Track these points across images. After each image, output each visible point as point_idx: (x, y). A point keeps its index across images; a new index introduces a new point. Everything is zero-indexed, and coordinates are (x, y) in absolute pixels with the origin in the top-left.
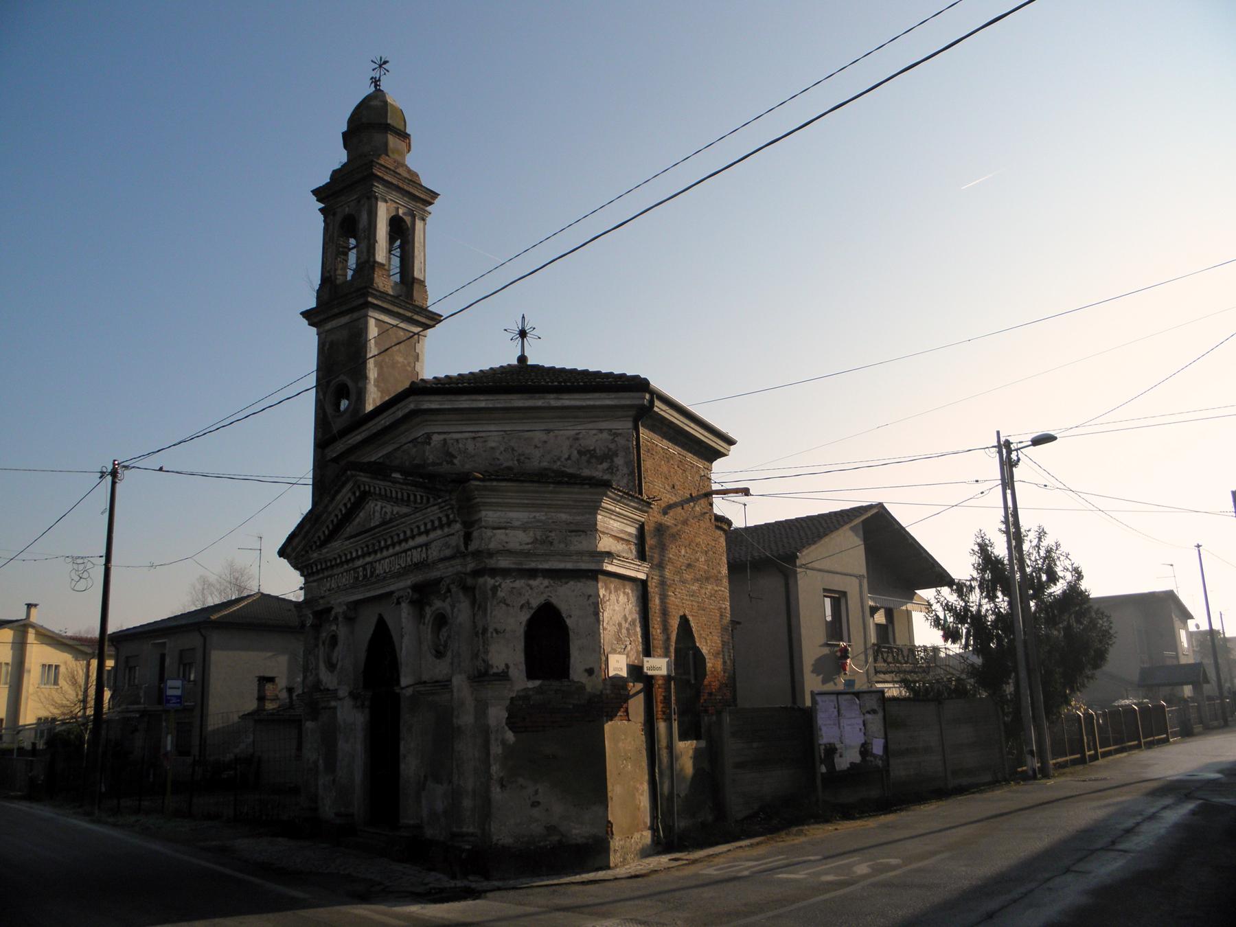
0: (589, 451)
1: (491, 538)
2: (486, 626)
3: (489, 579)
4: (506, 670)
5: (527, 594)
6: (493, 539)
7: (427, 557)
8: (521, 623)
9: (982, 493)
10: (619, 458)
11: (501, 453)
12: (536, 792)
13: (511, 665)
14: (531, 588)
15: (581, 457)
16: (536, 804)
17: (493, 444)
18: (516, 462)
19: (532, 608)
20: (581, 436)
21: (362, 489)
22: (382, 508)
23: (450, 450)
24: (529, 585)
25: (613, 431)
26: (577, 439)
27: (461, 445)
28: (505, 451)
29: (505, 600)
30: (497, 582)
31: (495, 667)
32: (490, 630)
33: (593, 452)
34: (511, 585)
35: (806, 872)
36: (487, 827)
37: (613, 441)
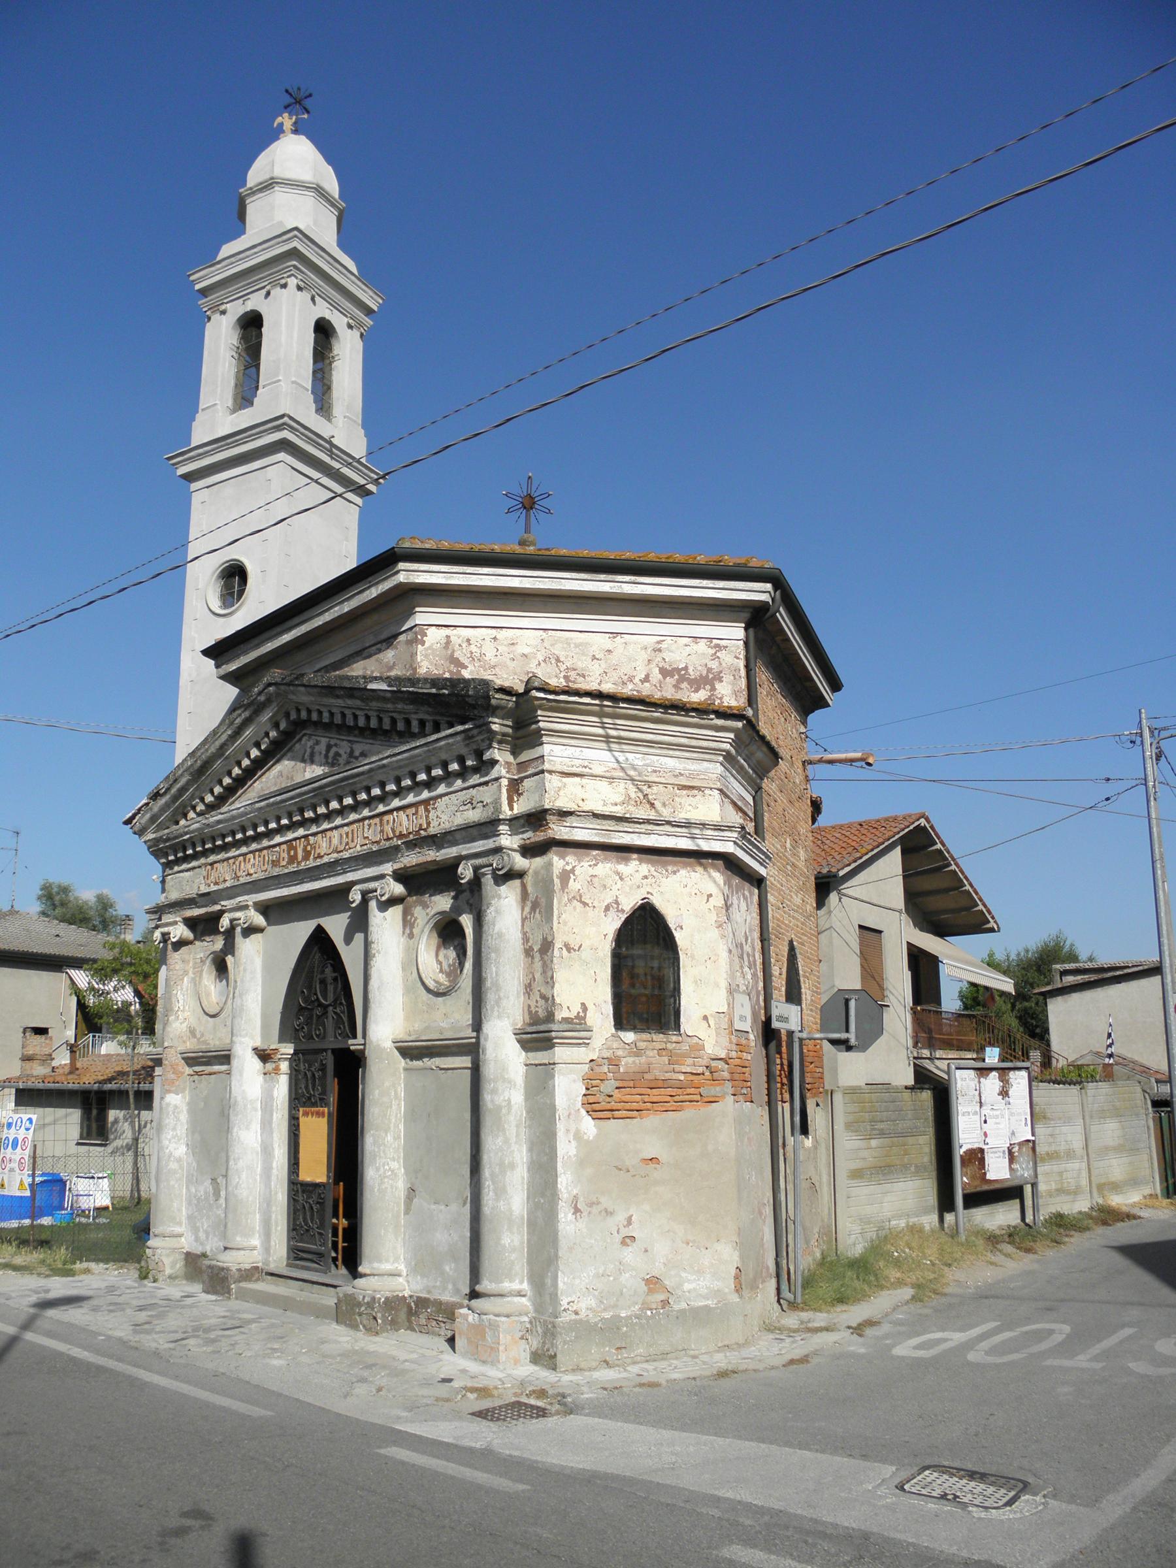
0: (678, 670)
1: (560, 789)
2: (549, 939)
3: (555, 859)
4: (582, 1014)
5: (615, 888)
6: (561, 793)
7: (428, 824)
8: (605, 936)
9: (1107, 799)
10: (724, 683)
11: (539, 664)
12: (629, 1221)
13: (590, 1006)
14: (621, 879)
15: (665, 678)
16: (628, 1240)
17: (526, 650)
18: (562, 680)
19: (623, 911)
20: (663, 646)
21: (293, 716)
22: (329, 747)
23: (456, 655)
24: (618, 873)
25: (715, 641)
26: (660, 650)
27: (473, 648)
28: (545, 661)
29: (581, 896)
30: (567, 863)
31: (565, 1007)
32: (558, 944)
33: (683, 672)
34: (592, 871)
35: (1097, 1349)
36: (549, 1281)
37: (715, 657)
